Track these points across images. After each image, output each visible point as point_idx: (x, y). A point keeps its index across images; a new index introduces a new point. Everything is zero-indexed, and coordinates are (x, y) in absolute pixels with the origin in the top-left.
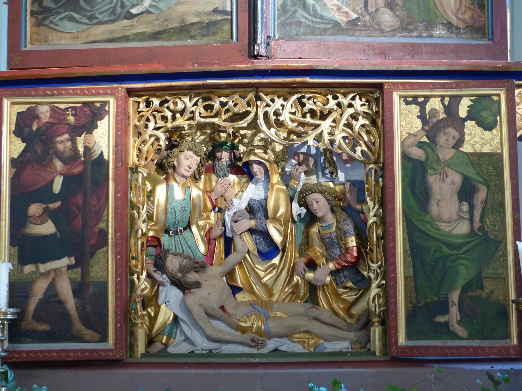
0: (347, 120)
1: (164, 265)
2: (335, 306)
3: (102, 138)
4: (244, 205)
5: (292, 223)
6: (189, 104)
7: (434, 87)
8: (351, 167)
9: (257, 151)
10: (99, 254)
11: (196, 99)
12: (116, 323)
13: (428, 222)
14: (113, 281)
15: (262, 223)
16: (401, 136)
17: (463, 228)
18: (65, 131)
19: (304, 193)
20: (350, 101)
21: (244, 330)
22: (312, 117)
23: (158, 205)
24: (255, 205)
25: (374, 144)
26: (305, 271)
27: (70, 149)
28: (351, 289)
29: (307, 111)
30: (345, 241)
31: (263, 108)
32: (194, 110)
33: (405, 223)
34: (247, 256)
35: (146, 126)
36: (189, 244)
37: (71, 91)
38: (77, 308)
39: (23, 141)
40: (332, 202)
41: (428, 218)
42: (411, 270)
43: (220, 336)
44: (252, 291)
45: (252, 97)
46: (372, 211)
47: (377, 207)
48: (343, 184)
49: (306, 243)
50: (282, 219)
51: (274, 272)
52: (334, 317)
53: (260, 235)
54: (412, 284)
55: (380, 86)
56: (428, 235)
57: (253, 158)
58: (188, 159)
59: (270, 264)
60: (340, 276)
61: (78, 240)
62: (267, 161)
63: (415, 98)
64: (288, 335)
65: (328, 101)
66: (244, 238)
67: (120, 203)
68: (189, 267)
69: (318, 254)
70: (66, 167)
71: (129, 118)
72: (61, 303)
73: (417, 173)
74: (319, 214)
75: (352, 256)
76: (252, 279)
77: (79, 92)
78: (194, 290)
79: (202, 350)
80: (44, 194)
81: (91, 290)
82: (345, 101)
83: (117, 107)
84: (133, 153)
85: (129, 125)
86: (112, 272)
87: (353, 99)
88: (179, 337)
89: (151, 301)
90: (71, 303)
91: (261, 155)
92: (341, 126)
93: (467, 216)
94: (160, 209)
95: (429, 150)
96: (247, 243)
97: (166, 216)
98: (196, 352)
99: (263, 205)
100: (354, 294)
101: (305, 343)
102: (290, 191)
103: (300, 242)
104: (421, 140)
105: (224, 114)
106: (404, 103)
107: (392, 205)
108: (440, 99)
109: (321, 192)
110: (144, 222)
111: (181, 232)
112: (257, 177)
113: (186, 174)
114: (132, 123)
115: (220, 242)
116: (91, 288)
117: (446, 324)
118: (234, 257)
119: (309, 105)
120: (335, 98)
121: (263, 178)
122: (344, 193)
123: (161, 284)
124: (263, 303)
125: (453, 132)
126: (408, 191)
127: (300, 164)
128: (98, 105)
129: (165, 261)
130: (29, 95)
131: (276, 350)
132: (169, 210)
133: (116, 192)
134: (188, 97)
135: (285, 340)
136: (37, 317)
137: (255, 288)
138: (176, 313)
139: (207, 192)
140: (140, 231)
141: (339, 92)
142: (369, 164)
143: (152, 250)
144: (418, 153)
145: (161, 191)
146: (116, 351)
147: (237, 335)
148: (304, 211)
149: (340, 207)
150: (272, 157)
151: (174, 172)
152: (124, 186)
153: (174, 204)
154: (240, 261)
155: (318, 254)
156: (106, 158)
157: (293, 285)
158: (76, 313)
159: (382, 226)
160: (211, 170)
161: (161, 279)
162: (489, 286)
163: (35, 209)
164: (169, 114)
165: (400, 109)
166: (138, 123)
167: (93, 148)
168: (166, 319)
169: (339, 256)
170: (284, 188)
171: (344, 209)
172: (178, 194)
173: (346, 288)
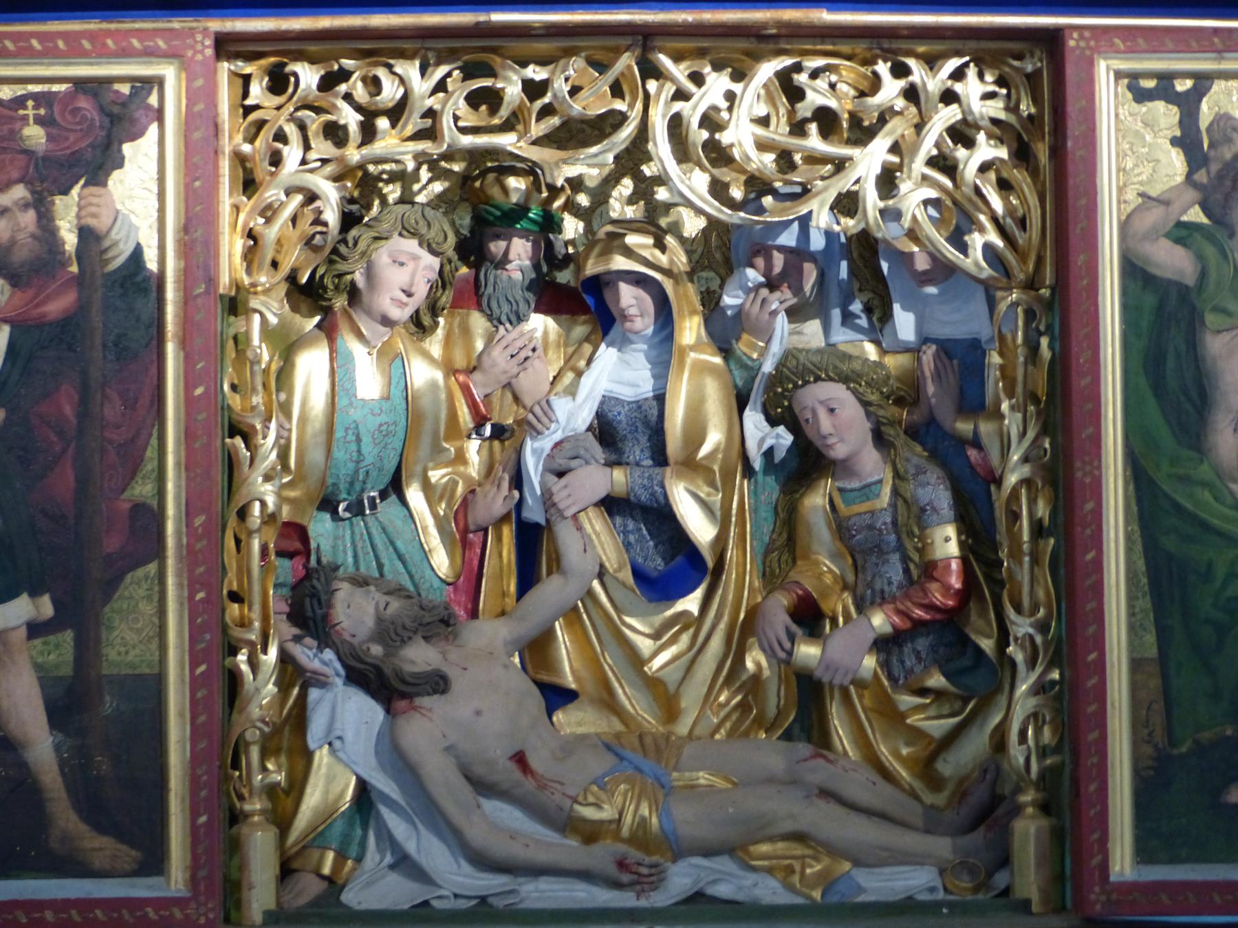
0: (937, 145)
1: (326, 617)
2: (884, 750)
3: (137, 199)
5: (744, 476)
6: (420, 86)
8: (940, 294)
9: (632, 239)
10: (136, 583)
11: (442, 70)
12: (194, 813)
13: (1205, 484)
14: (182, 675)
15: (650, 478)
16: (1119, 202)
18: (15, 174)
19: (789, 380)
20: (949, 83)
21: (590, 833)
22: (825, 134)
23: (303, 419)
24: (621, 417)
25: (1022, 223)
26: (792, 638)
27: (33, 236)
29: (809, 114)
30: (922, 538)
31: (668, 104)
32: (437, 107)
33: (1131, 487)
34: (596, 584)
35: (276, 160)
36: (399, 544)
37: (35, 43)
38: (62, 764)
40: (881, 412)
42: (1150, 638)
43: (501, 848)
44: (609, 703)
45: (629, 67)
46: (1010, 443)
47: (1031, 434)
48: (906, 349)
49: (787, 539)
50: (716, 468)
51: (685, 638)
52: (887, 789)
53: (639, 517)
54: (1155, 683)
55: (1052, 40)
56: (1205, 526)
57: (620, 263)
58: (402, 264)
59: (669, 613)
60: (901, 652)
62: (667, 272)
63: (1166, 78)
64: (733, 849)
65: (875, 83)
66: (587, 526)
67: (201, 417)
68: (408, 623)
69: (828, 579)
70: (21, 297)
74: (839, 451)
75: (947, 588)
77: (61, 44)
78: (425, 701)
79: (456, 896)
81: (109, 704)
82: (933, 82)
84: (232, 247)
86: (180, 646)
87: (958, 75)
91: (646, 254)
92: (919, 166)
94: (310, 430)
95: (1210, 251)
97: (329, 451)
98: (436, 904)
100: (946, 711)
101: (793, 872)
102: (736, 373)
103: (767, 539)
104: (1185, 218)
105: (538, 120)
106: (1130, 96)
107: (1091, 430)
109: (845, 379)
110: (267, 478)
111: (373, 506)
112: (628, 324)
115: (499, 539)
116: (108, 698)
118: (551, 591)
119: (816, 96)
120: (900, 71)
121: (650, 331)
124: (648, 740)
126: (1143, 382)
127: (772, 284)
128: (125, 89)
129: (330, 605)
132: (339, 434)
134: (417, 63)
135: (724, 864)
137: (620, 691)
138: (366, 776)
139: (456, 372)
140: (256, 508)
142: (1009, 289)
143: (286, 569)
144: (1173, 261)
145: (312, 366)
146: (193, 905)
147: (568, 849)
148: (784, 438)
149: (900, 422)
151: (349, 304)
153: (356, 414)
154: (571, 605)
155: (828, 579)
156: (152, 265)
157: (744, 683)
158: (60, 779)
159: (1048, 491)
160: (474, 295)
161: (316, 665)
164: (350, 118)
165: (1117, 115)
166: (246, 148)
167: (109, 232)
168: (331, 797)
169: (900, 587)
170: (718, 360)
171: (913, 433)
172: (368, 381)
173: (922, 692)
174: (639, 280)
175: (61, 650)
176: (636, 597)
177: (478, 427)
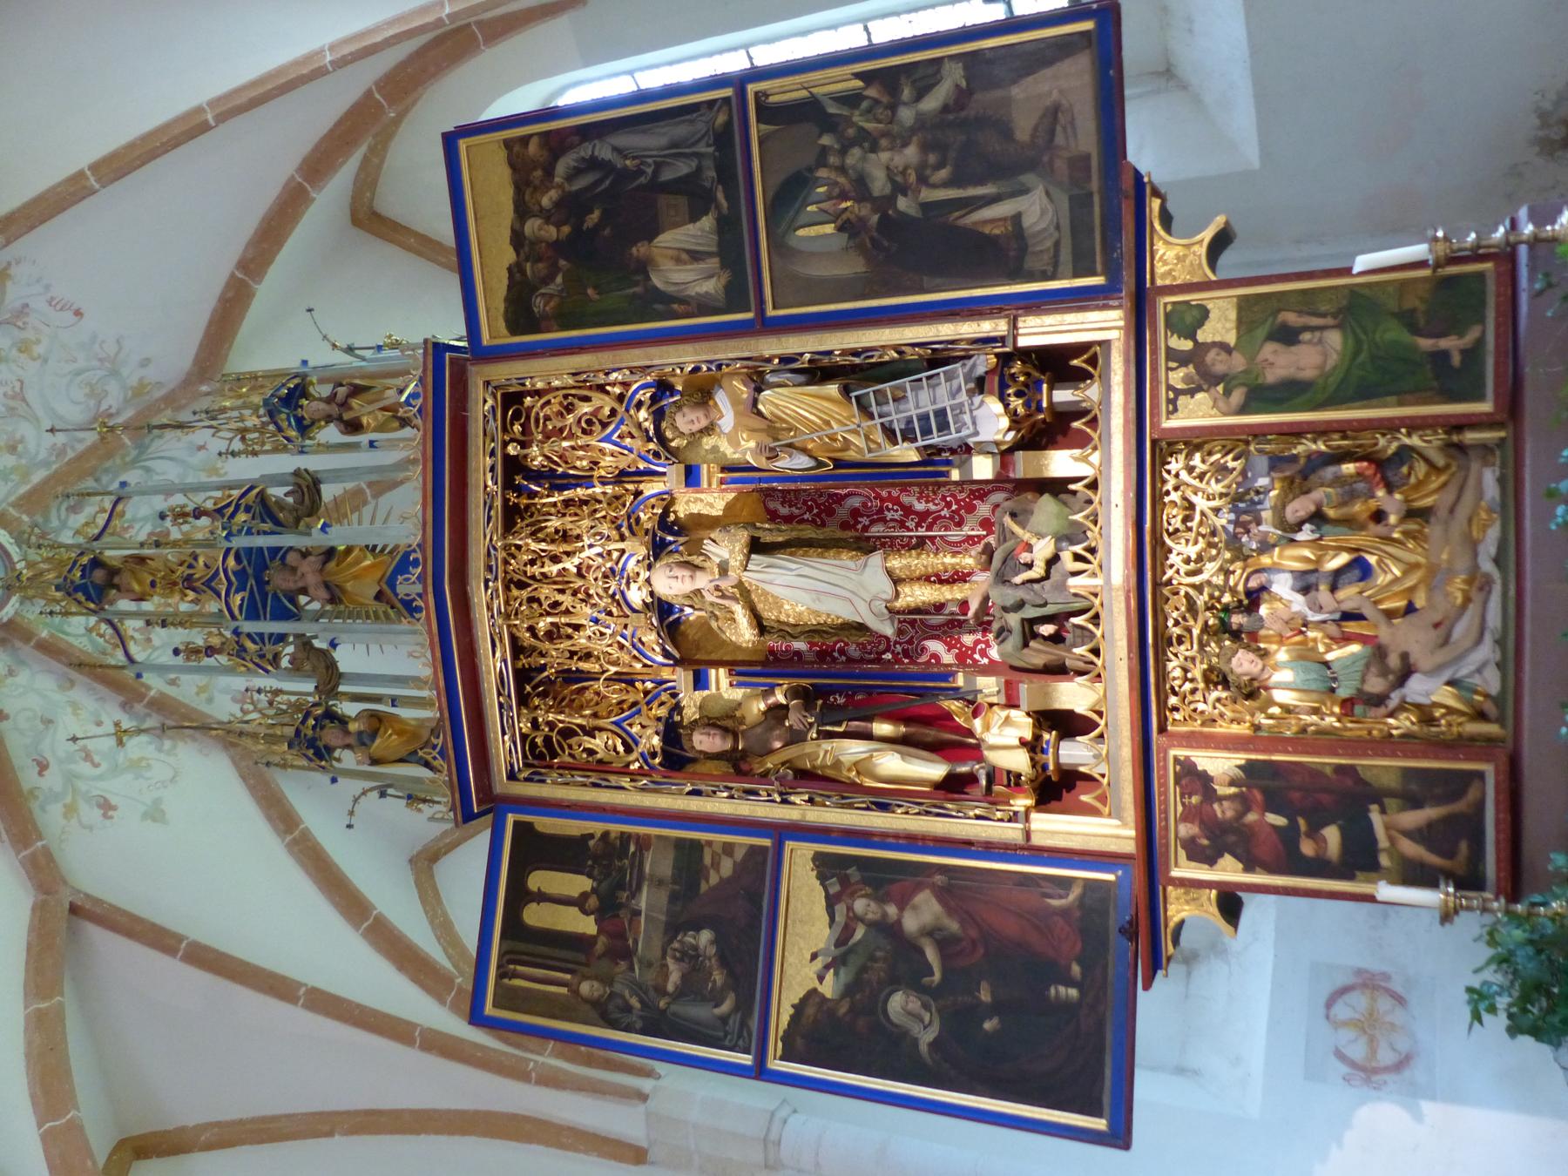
3: (1219, 765)
4: (1300, 598)
7: (1155, 379)
17: (1334, 339)
21: (1467, 600)
28: (1411, 468)
35: (1202, 712)
39: (1222, 856)
41: (1321, 381)
42: (1389, 399)
44: (1412, 589)
49: (1349, 523)
51: (1388, 562)
54: (1408, 397)
55: (1154, 442)
57: (1240, 588)
61: (1349, 799)
63: (1169, 401)
65: (1174, 503)
71: (1193, 733)
72: (1431, 825)
73: (1261, 396)
74: (1312, 508)
76: (1396, 588)
78: (1412, 660)
80: (1289, 837)
83: (1180, 746)
84: (1235, 729)
85: (1201, 733)
87: (1169, 472)
88: (1476, 680)
89: (1426, 714)
90: (1429, 813)
92: (1203, 486)
93: (1317, 334)
95: (1234, 382)
96: (1349, 595)
99: (1299, 575)
109: (1284, 507)
113: (1260, 667)
114: (1199, 729)
117: (1464, 352)
119: (1177, 523)
120: (1168, 493)
122: (1283, 479)
123: (1403, 701)
125: (1211, 356)
127: (1248, 532)
130: (1167, 845)
131: (1497, 561)
133: (1286, 752)
135: (1481, 549)
136: (1450, 854)
143: (1358, 709)
144: (1238, 396)
145: (1280, 696)
147: (1473, 609)
148: (1307, 527)
150: (1239, 564)
152: (1276, 742)
160: (1254, 636)
162: (1411, 302)
163: (1307, 848)
164: (1188, 686)
171: (1305, 478)
173: (1409, 474)
174: (1247, 580)
175: (1390, 803)
176: (1370, 582)
177: (1301, 632)
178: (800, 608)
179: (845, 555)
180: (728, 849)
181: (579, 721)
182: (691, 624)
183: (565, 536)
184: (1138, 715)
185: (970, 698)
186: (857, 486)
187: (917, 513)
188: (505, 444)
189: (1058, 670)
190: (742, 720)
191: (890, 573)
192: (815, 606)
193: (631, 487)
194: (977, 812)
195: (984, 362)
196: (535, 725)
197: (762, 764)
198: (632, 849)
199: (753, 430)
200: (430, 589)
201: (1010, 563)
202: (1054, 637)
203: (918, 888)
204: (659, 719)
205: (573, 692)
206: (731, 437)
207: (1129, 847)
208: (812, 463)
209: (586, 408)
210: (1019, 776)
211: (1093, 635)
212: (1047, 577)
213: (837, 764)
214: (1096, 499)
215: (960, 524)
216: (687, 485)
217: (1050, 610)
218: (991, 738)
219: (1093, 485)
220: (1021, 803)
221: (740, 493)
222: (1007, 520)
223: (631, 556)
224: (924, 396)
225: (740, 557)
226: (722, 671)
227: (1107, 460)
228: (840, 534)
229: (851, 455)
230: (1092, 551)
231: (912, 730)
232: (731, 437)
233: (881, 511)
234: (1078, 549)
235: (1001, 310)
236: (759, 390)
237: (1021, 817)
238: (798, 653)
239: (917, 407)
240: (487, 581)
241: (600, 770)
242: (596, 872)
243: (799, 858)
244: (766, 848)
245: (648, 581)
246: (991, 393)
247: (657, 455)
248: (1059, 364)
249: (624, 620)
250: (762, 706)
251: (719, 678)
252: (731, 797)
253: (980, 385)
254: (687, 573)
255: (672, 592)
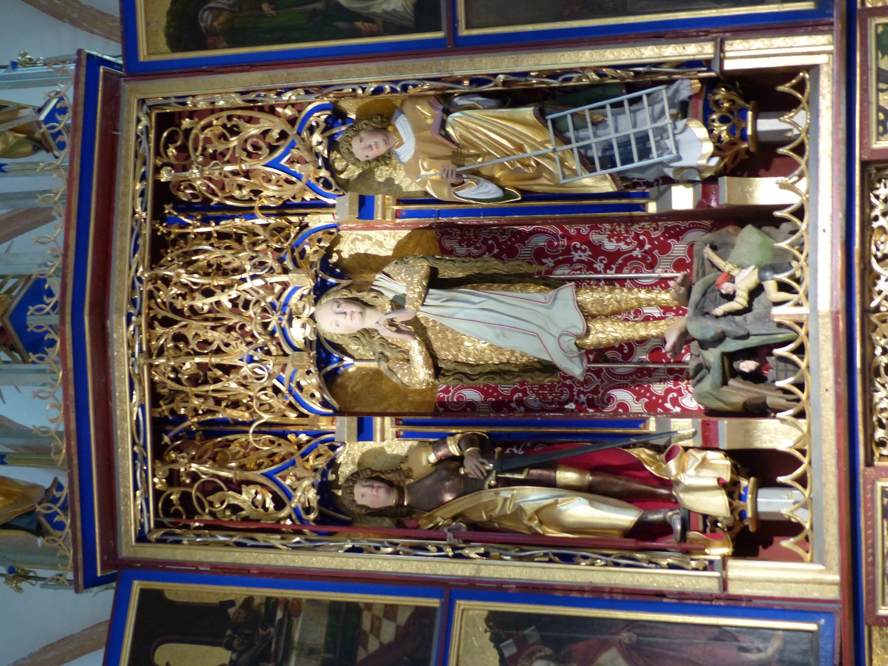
55: (864, 164)
87: (877, 197)
108: (881, 94)
120: (876, 218)
141: (869, 215)
178: (481, 345)
179: (532, 289)
180: (391, 611)
181: (224, 474)
182: (351, 377)
183: (221, 270)
184: (845, 444)
185: (661, 442)
186: (545, 222)
187: (608, 254)
188: (157, 170)
189: (761, 410)
190: (408, 474)
191: (581, 307)
192: (499, 343)
193: (294, 219)
194: (670, 561)
195: (688, 87)
196: (173, 479)
197: (430, 519)
198: (279, 615)
199: (436, 158)
200: (68, 319)
201: (710, 296)
202: (756, 367)
203: (604, 646)
204: (316, 470)
205: (216, 445)
206: (411, 164)
207: (833, 593)
208: (498, 193)
209: (253, 130)
210: (715, 522)
211: (797, 366)
212: (748, 309)
213: (519, 511)
214: (803, 226)
215: (652, 266)
216: (361, 217)
217: (752, 342)
218: (687, 479)
219: (799, 213)
220: (717, 551)
221: (416, 229)
222: (708, 252)
223: (295, 289)
224: (625, 120)
225: (419, 289)
226: (387, 420)
227: (814, 187)
228: (525, 268)
229: (542, 185)
230: (798, 281)
231: (598, 479)
232: (411, 164)
233: (567, 251)
234: (783, 277)
235: (707, 33)
236: (447, 112)
237: (718, 565)
238: (472, 405)
239: (616, 131)
240: (129, 316)
241: (251, 528)
242: (236, 642)
243: (471, 613)
244: (434, 609)
245: (312, 317)
246: (695, 117)
247: (327, 185)
248: (769, 91)
249: (282, 360)
250: (433, 458)
251: (384, 426)
252: (397, 553)
253: (683, 110)
254: (356, 309)
255: (339, 331)
